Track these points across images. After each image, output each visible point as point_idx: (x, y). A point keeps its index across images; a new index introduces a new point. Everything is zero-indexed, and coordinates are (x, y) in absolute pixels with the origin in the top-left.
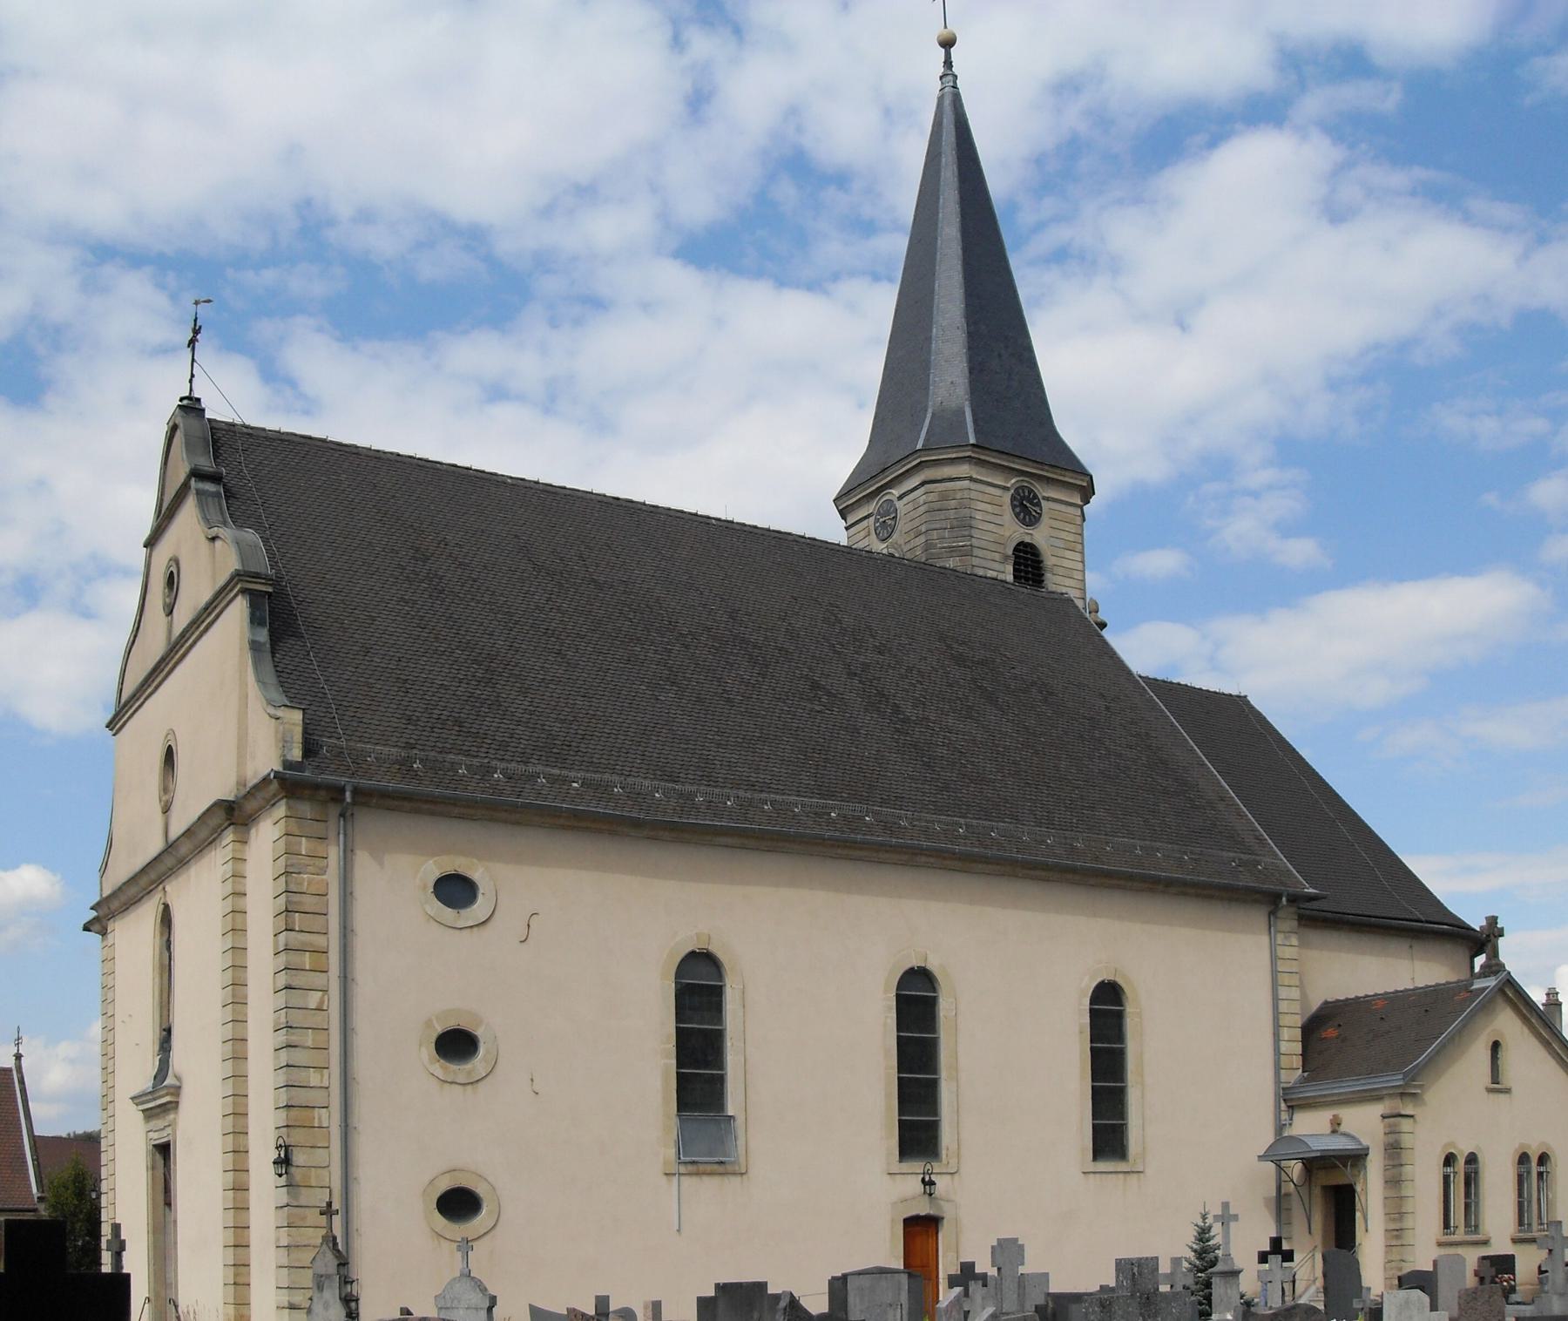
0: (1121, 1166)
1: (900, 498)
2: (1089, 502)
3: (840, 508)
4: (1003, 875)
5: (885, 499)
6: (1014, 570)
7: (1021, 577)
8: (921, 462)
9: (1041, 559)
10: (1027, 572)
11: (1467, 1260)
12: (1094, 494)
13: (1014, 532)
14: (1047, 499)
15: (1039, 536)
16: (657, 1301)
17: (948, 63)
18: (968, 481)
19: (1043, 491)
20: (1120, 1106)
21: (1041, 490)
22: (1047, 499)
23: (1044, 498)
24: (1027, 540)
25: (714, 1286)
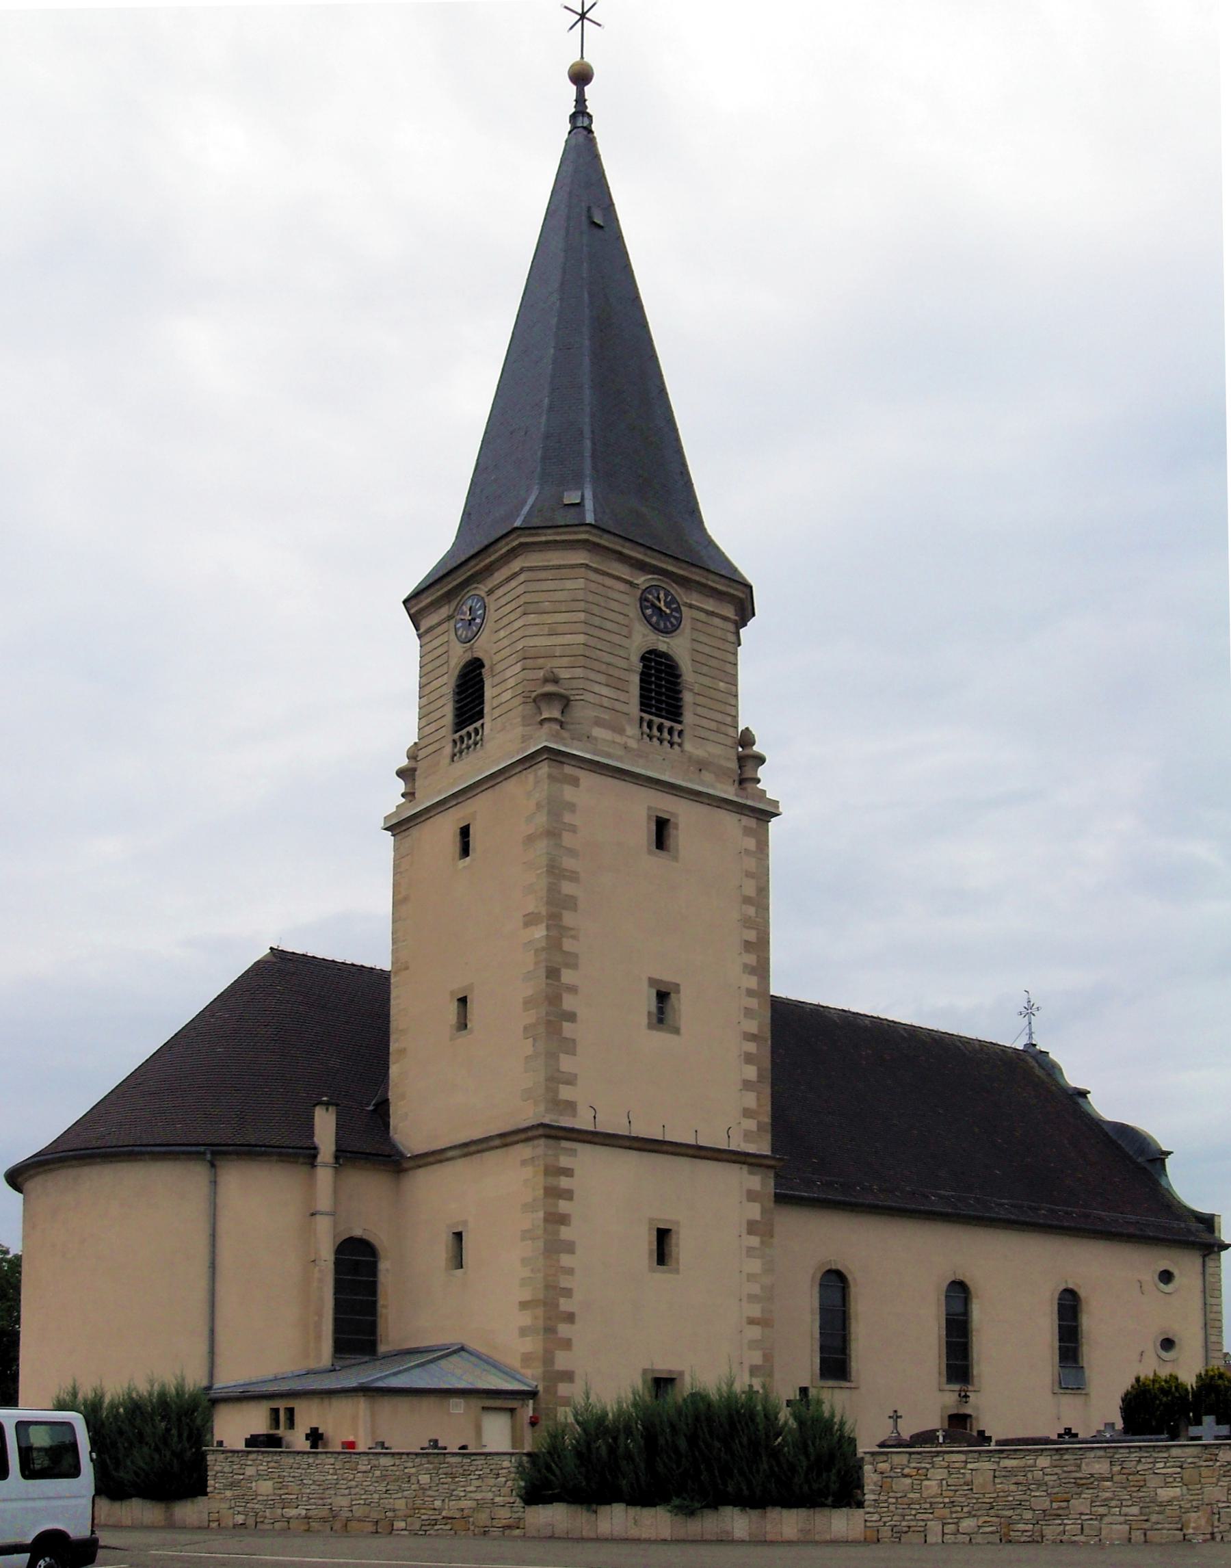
0: (848, 1384)
1: (490, 592)
2: (746, 625)
3: (412, 611)
4: (576, 904)
5: (473, 593)
6: (642, 681)
7: (650, 706)
8: (521, 544)
9: (681, 696)
10: (661, 702)
11: (1166, 1354)
12: (754, 615)
13: (642, 638)
14: (691, 606)
15: (679, 647)
16: (661, 1265)
17: (581, 101)
18: (583, 570)
19: (684, 596)
20: (808, 1505)
21: (683, 596)
22: (691, 606)
23: (686, 604)
24: (663, 648)
25: (659, 1266)
